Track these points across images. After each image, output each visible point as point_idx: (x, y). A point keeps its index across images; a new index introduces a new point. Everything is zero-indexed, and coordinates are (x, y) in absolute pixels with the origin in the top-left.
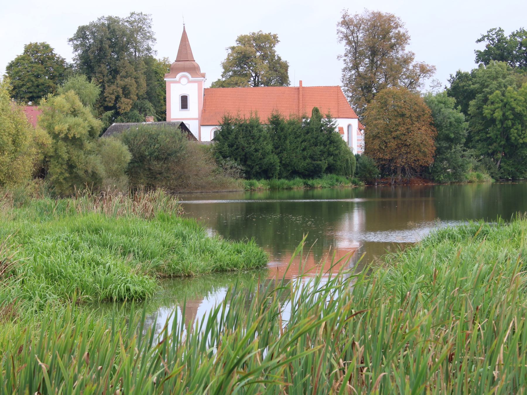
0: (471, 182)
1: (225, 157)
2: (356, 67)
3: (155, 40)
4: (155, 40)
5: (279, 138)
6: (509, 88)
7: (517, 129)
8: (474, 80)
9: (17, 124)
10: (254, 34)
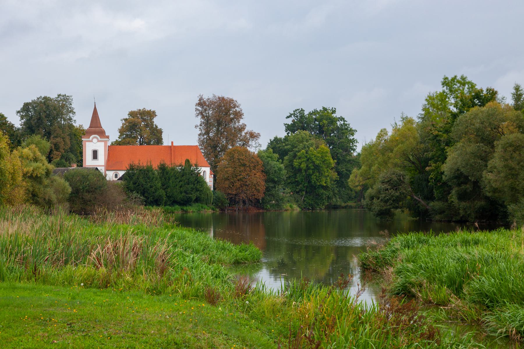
0: (286, 210)
1: (132, 191)
2: (207, 133)
3: (75, 113)
4: (75, 113)
5: (165, 179)
6: (311, 148)
7: (316, 175)
8: (287, 143)
9: (14, 165)
10: (140, 110)
